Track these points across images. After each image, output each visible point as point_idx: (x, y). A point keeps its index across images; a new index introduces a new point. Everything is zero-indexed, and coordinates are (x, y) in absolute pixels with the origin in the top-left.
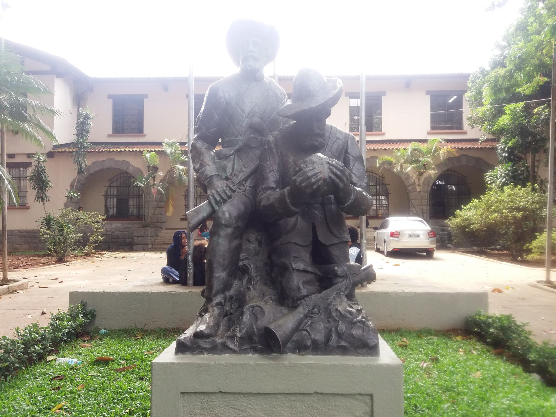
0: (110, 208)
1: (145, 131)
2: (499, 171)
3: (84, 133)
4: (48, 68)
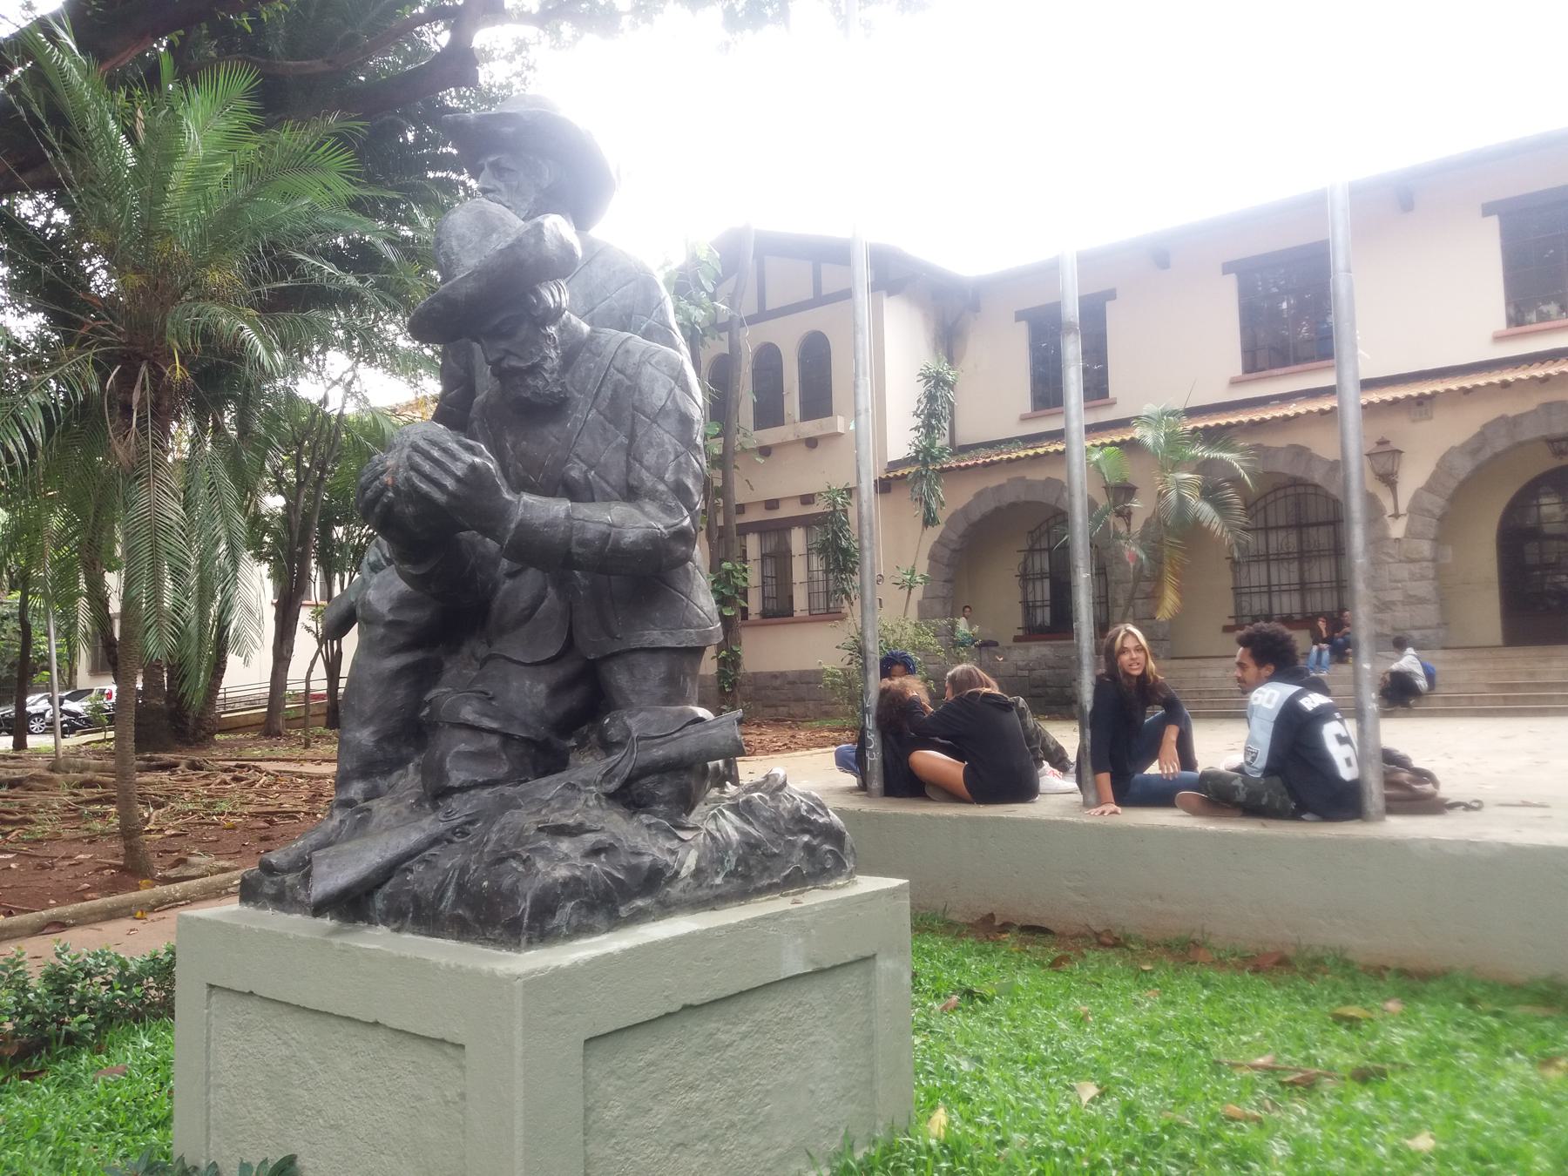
0: (1035, 607)
1: (1114, 391)
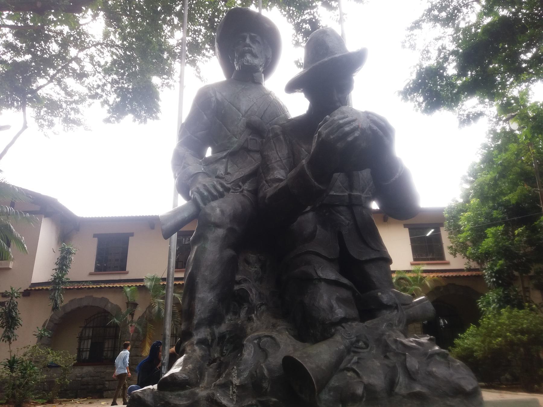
0: (83, 351)
1: (128, 269)
2: (491, 296)
3: (64, 267)
4: (37, 208)
